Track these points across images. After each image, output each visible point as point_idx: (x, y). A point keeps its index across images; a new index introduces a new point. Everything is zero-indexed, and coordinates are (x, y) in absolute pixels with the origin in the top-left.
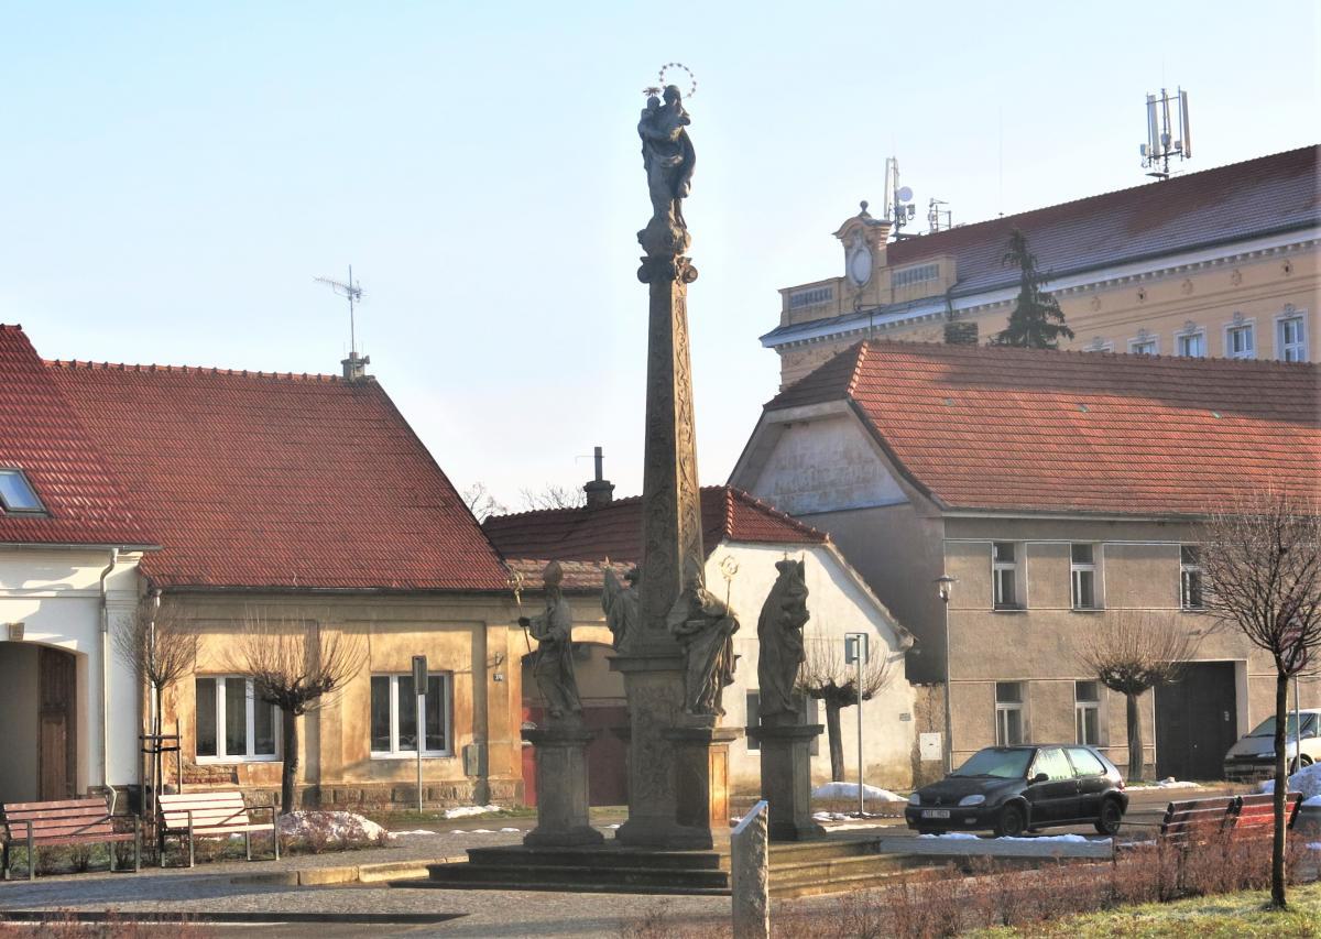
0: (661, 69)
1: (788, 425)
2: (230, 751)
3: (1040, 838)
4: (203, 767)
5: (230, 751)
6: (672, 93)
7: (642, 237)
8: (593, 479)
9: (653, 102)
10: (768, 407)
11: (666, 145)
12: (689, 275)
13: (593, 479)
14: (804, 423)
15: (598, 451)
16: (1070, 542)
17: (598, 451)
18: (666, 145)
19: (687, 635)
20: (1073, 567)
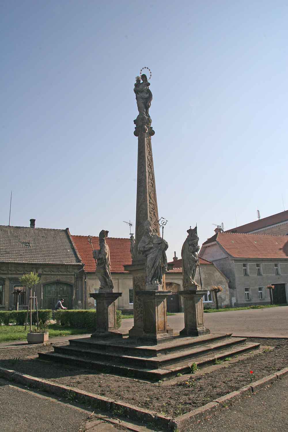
0: (142, 68)
1: (206, 247)
2: (205, 301)
3: (108, 256)
4: (132, 303)
5: (209, 300)
6: (144, 77)
7: (135, 122)
8: (174, 257)
9: (138, 80)
10: (203, 244)
11: (143, 93)
12: (152, 133)
13: (174, 257)
14: (209, 246)
15: (175, 252)
16: (256, 263)
17: (175, 252)
18: (143, 93)
19: (146, 251)
20: (257, 268)
